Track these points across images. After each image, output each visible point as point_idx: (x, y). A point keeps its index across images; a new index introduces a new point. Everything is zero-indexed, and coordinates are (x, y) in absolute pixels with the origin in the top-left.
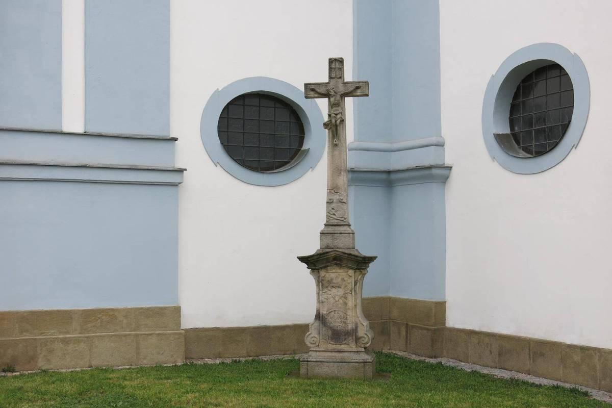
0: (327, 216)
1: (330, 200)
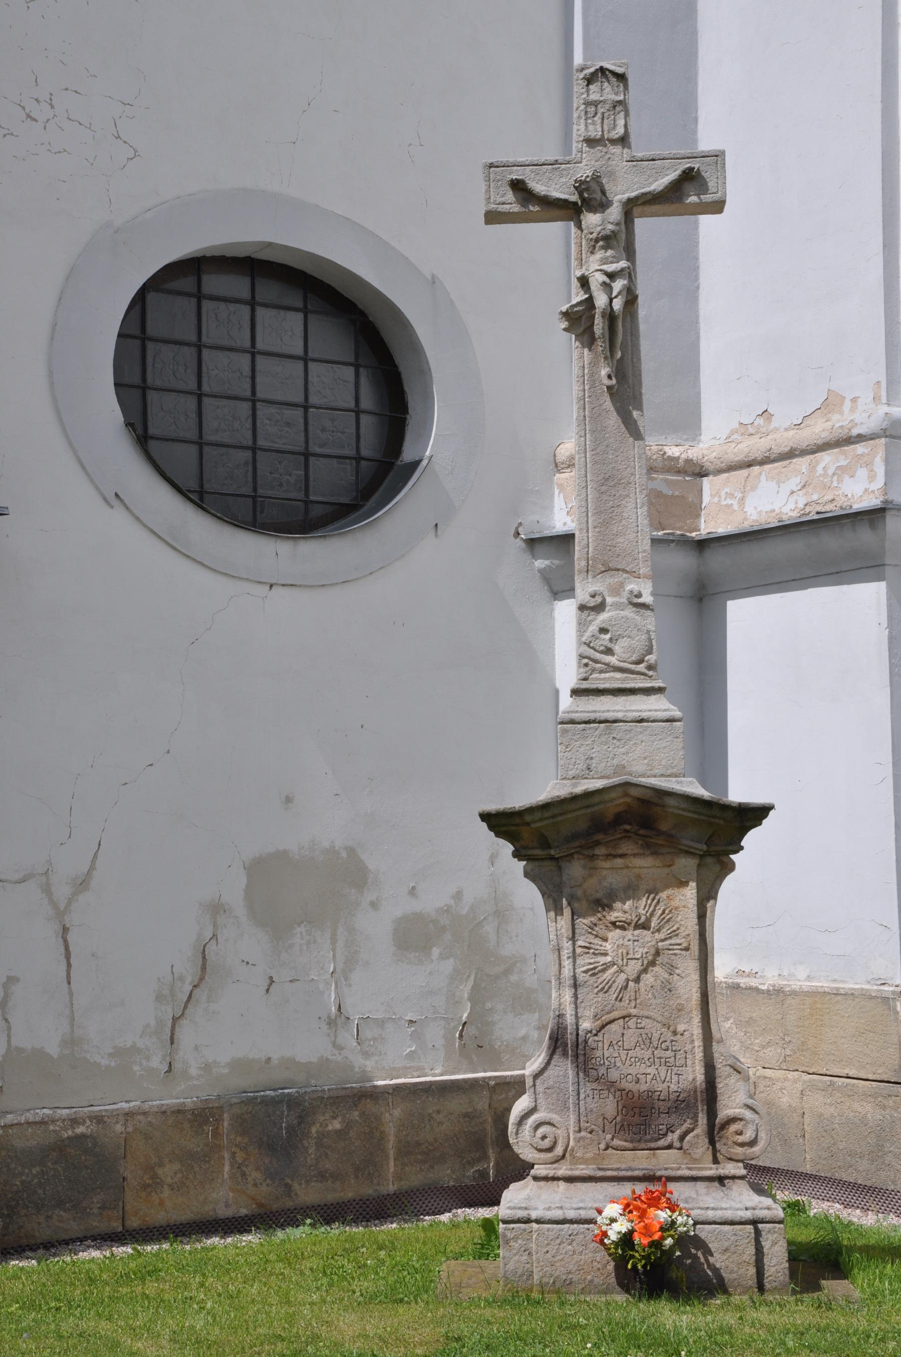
0: (581, 657)
1: (593, 596)
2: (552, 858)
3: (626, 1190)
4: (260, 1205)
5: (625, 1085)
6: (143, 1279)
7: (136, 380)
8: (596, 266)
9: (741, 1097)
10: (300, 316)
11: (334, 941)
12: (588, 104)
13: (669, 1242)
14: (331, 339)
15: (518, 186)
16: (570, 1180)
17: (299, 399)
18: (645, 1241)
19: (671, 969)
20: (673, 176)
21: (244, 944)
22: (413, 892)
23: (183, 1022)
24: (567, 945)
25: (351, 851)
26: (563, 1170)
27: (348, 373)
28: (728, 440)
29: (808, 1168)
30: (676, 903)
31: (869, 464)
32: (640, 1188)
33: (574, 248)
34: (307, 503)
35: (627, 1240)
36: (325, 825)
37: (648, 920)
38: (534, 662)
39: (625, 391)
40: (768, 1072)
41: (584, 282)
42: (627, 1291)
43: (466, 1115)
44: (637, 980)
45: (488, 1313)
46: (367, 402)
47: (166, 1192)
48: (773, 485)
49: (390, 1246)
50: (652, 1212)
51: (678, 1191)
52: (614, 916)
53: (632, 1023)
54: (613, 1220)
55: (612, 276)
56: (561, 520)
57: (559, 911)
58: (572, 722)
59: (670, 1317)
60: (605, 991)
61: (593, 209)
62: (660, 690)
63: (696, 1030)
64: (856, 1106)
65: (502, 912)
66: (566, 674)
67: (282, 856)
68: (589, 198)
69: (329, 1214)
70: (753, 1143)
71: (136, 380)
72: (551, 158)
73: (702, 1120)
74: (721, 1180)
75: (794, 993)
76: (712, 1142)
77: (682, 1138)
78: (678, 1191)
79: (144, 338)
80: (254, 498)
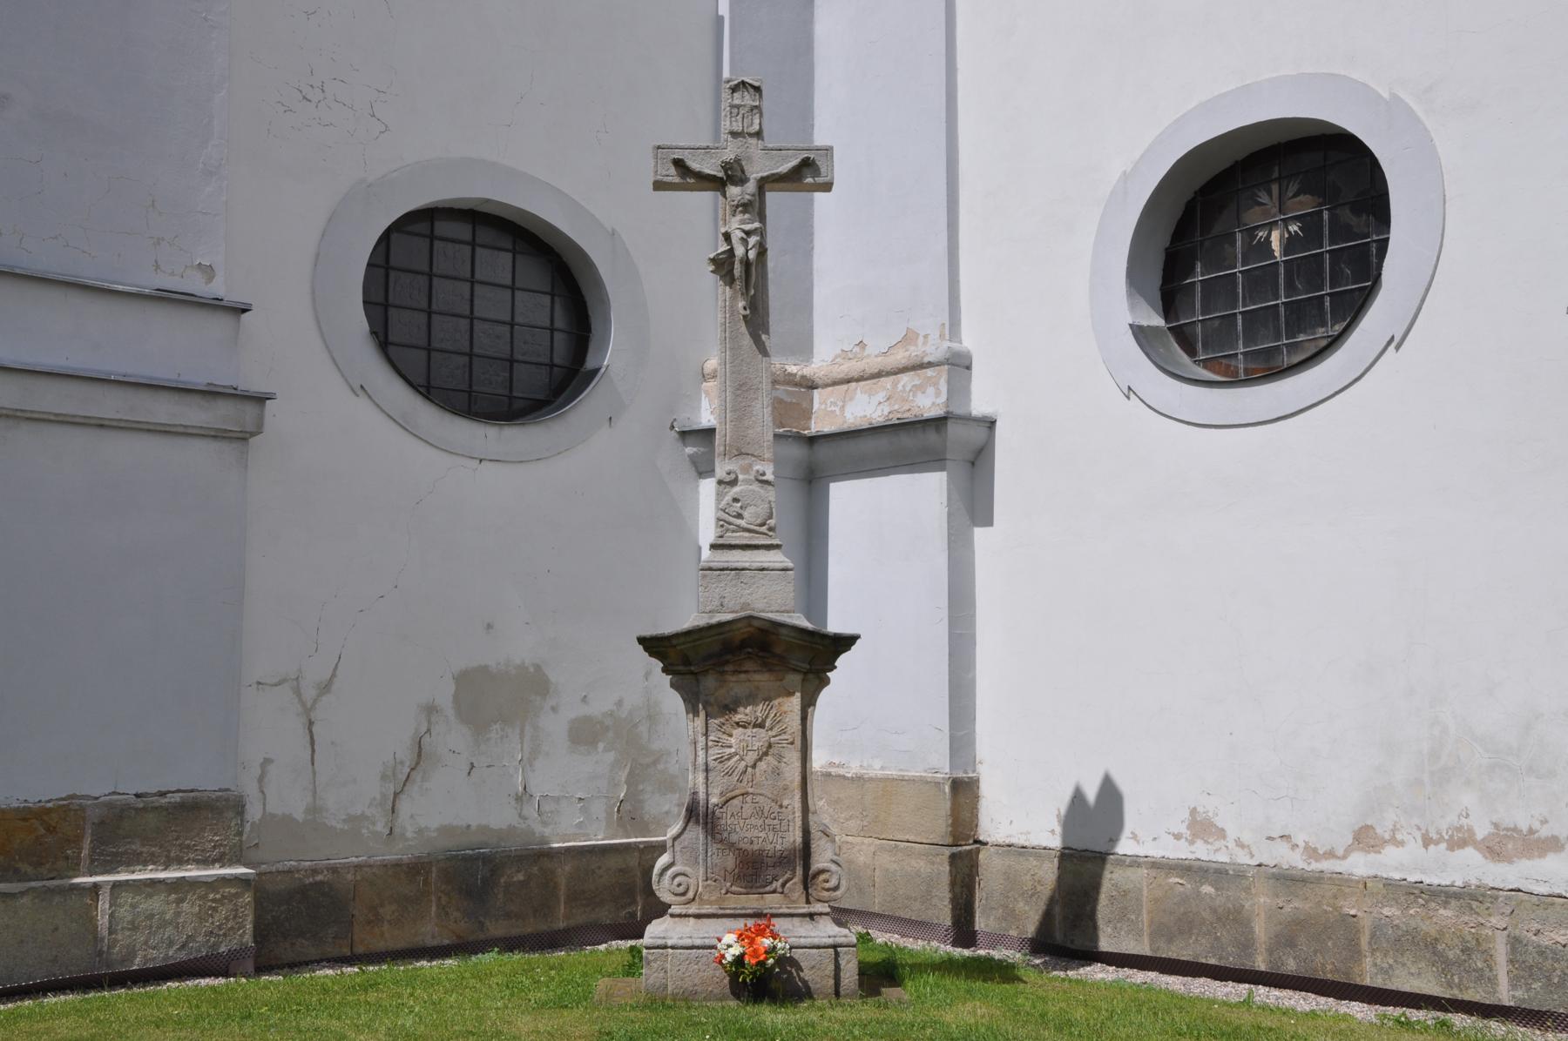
0: (719, 519)
2: (692, 673)
3: (740, 924)
4: (459, 937)
5: (742, 845)
6: (366, 990)
7: (381, 299)
8: (736, 225)
9: (829, 855)
10: (510, 255)
11: (522, 731)
12: (732, 106)
13: (771, 961)
14: (533, 273)
15: (679, 164)
16: (698, 916)
17: (508, 318)
18: (754, 961)
19: (780, 758)
20: (794, 162)
21: (452, 738)
22: (584, 699)
23: (403, 796)
24: (702, 740)
25: (538, 667)
26: (693, 909)
27: (547, 300)
28: (833, 363)
29: (876, 909)
30: (785, 708)
31: (936, 384)
32: (751, 922)
33: (721, 212)
34: (510, 398)
35: (739, 960)
36: (519, 647)
37: (764, 721)
38: (684, 526)
39: (756, 320)
40: (850, 839)
41: (727, 237)
42: (738, 998)
43: (621, 870)
44: (754, 766)
45: (632, 1015)
46: (560, 323)
47: (386, 927)
48: (866, 397)
49: (560, 967)
50: (759, 939)
51: (779, 924)
52: (737, 717)
53: (749, 799)
54: (729, 946)
55: (748, 233)
56: (706, 417)
57: (696, 713)
58: (710, 569)
59: (770, 1016)
60: (729, 774)
61: (735, 184)
62: (778, 547)
63: (797, 804)
64: (913, 863)
65: (653, 716)
66: (707, 533)
67: (484, 669)
68: (732, 174)
69: (510, 944)
70: (836, 888)
71: (381, 299)
72: (704, 145)
73: (799, 871)
74: (811, 916)
75: (871, 779)
76: (806, 888)
77: (783, 885)
78: (779, 924)
79: (387, 268)
80: (470, 393)
